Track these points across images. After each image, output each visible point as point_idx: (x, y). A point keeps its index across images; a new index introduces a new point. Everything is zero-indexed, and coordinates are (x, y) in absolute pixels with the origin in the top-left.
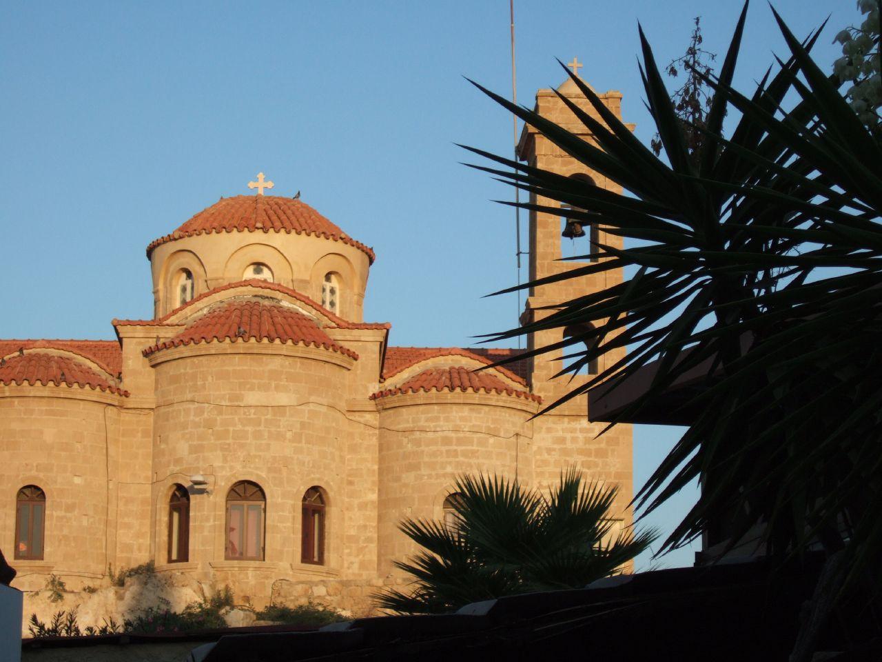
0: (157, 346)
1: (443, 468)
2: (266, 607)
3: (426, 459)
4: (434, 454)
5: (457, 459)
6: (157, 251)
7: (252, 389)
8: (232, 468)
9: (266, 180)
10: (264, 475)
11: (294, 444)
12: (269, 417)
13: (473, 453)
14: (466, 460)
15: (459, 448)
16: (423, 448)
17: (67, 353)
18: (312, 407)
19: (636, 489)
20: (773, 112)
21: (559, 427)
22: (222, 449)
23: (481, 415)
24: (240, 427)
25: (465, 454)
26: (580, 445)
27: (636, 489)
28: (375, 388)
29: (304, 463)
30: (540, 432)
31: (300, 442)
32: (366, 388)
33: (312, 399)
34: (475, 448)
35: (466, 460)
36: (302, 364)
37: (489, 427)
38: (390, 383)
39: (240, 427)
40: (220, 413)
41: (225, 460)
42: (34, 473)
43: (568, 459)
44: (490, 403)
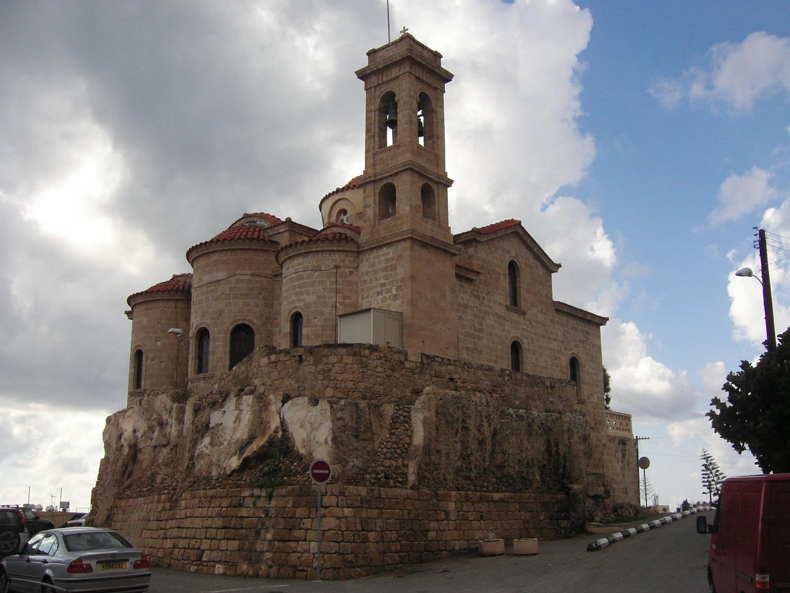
2: (65, 505)
5: (296, 291)
11: (225, 301)
12: (212, 288)
16: (203, 297)
17: (463, 274)
18: (237, 277)
19: (744, 464)
21: (372, 256)
23: (309, 259)
26: (383, 265)
27: (744, 464)
29: (231, 311)
30: (362, 262)
33: (237, 273)
34: (305, 281)
36: (231, 253)
37: (314, 266)
43: (376, 276)
44: (311, 250)
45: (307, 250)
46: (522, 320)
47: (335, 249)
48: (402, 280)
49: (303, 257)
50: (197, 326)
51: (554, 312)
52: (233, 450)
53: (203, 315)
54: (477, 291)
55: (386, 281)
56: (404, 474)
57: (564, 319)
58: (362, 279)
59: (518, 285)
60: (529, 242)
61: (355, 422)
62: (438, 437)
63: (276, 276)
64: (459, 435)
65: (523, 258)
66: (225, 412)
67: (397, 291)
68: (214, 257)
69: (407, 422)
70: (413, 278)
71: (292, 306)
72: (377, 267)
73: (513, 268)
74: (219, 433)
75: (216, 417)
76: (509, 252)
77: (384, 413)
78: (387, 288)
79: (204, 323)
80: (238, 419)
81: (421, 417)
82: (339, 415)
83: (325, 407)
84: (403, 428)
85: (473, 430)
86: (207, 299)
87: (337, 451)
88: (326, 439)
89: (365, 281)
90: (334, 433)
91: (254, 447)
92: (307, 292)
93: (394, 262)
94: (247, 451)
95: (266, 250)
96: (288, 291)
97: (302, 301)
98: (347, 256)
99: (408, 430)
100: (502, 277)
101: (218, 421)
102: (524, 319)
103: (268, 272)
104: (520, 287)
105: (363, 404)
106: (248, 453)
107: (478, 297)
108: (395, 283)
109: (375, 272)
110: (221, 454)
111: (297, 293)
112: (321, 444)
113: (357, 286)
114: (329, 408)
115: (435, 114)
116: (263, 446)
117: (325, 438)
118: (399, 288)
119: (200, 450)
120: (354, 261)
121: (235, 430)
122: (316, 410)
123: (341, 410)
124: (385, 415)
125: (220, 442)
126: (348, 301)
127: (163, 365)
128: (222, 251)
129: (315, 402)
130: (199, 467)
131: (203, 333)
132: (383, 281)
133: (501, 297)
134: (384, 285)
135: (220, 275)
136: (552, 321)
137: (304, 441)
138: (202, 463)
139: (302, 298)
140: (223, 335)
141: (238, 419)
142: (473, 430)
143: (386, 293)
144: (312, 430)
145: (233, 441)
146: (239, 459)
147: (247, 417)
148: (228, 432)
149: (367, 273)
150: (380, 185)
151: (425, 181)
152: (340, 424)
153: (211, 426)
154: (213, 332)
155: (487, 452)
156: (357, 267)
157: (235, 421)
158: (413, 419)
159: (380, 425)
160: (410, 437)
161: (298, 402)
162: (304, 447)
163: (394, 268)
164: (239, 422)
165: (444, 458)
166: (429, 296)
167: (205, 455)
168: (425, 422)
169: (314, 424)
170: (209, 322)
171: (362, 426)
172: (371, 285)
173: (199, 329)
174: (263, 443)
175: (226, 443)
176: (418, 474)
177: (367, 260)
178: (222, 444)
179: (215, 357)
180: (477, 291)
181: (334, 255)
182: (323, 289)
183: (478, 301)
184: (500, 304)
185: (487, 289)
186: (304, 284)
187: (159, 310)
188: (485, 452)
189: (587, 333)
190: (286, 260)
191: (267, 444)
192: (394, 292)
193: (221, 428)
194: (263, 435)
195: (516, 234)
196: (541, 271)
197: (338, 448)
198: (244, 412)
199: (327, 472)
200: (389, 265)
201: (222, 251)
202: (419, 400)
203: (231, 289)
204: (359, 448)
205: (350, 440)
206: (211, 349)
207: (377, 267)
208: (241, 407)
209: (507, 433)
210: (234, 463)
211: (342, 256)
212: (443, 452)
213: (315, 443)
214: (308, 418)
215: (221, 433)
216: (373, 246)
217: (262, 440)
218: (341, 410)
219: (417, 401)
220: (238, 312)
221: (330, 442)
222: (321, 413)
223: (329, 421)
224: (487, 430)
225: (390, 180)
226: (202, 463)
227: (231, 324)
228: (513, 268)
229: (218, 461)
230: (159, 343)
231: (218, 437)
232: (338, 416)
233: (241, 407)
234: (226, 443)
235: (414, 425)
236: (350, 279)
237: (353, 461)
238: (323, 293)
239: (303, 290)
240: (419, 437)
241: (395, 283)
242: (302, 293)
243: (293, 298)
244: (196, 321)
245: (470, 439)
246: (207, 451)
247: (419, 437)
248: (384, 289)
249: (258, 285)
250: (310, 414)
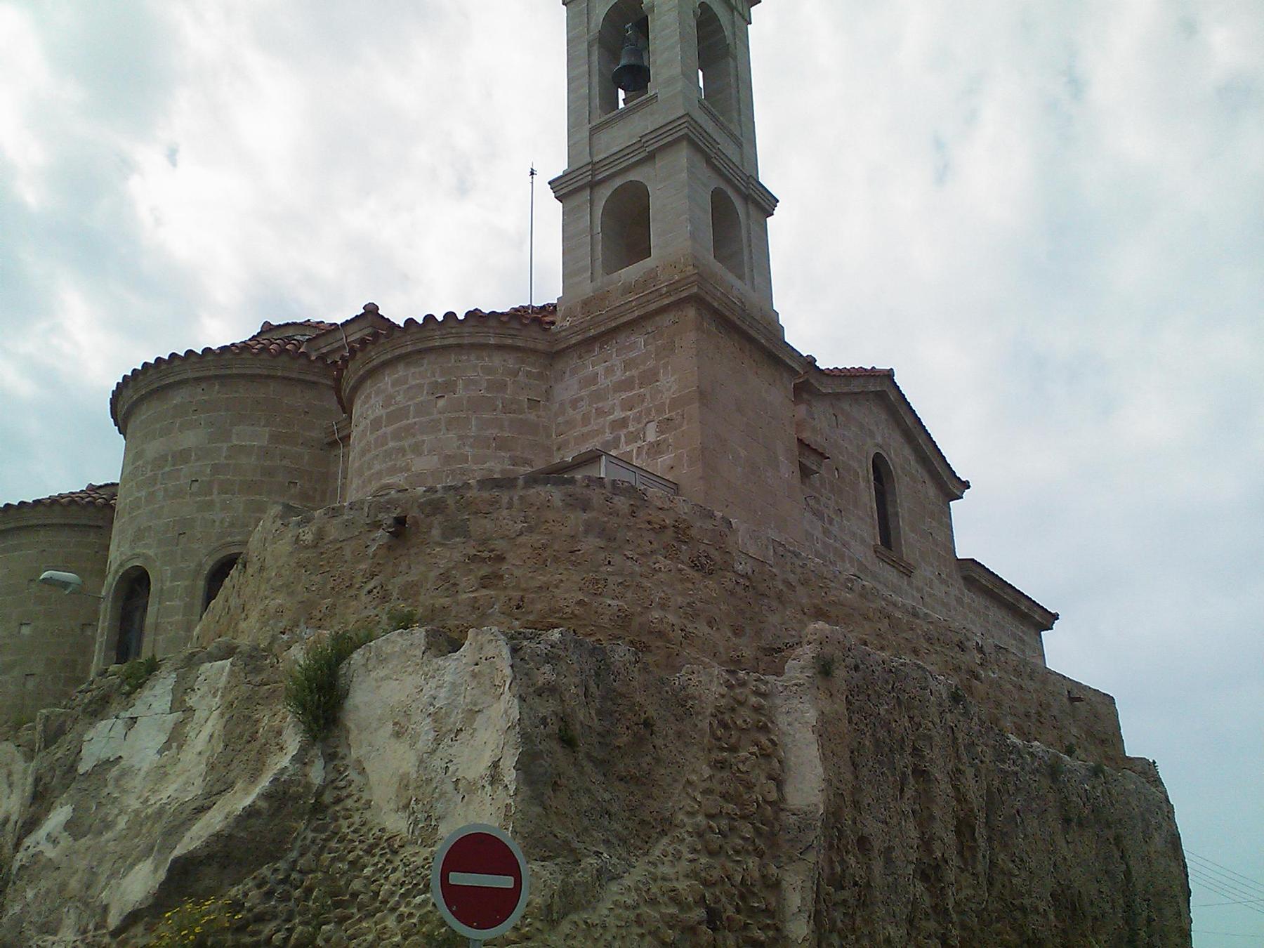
15: (390, 429)
26: (619, 375)
43: (600, 405)
44: (431, 344)
45: (420, 346)
46: (905, 586)
47: (492, 341)
48: (675, 404)
49: (408, 365)
50: (121, 565)
51: (962, 581)
52: (142, 842)
53: (139, 536)
54: (818, 501)
55: (629, 413)
56: (768, 912)
57: (979, 602)
58: (560, 419)
59: (890, 510)
60: (909, 421)
61: (599, 712)
62: (856, 790)
63: (333, 444)
64: (909, 793)
65: (900, 457)
66: (134, 720)
67: (661, 432)
68: (178, 398)
69: (764, 729)
70: (703, 396)
71: (375, 485)
72: (604, 382)
73: (880, 469)
74: (106, 791)
75: (99, 741)
76: (872, 434)
77: (690, 691)
78: (631, 429)
79: (138, 556)
80: (176, 739)
81: (811, 716)
82: (545, 674)
83: (490, 650)
84: (755, 749)
85: (943, 787)
86: (151, 497)
87: (539, 810)
88: (495, 765)
89: (570, 423)
90: (526, 737)
91: (214, 821)
92: (417, 449)
93: (651, 363)
94: (186, 839)
95: (314, 383)
96: (363, 453)
97: (401, 470)
98: (523, 362)
99: (767, 756)
100: (862, 484)
101: (108, 753)
102: (910, 584)
103: (316, 434)
104: (897, 514)
105: (621, 654)
106: (192, 840)
107: (818, 514)
108: (653, 413)
109: (598, 396)
110: (100, 862)
112: (472, 788)
113: (549, 436)
114: (506, 652)
115: (732, 63)
116: (251, 812)
117: (487, 761)
118: (665, 425)
119: (32, 851)
120: (540, 376)
121: (160, 774)
122: (453, 666)
123: (550, 659)
124: (693, 698)
125: (103, 820)
127: (31, 684)
128: (198, 380)
129: (446, 642)
130: (17, 909)
131: (136, 585)
132: (618, 414)
133: (860, 528)
134: (623, 423)
135: (190, 439)
136: (959, 600)
137: (404, 783)
138: (30, 894)
139: (401, 463)
140: (187, 583)
141: (176, 739)
142: (943, 787)
143: (627, 443)
144: (438, 741)
145: (150, 811)
146: (156, 870)
147: (207, 728)
148: (136, 783)
149: (574, 403)
150: (605, 193)
151: (723, 186)
152: (547, 707)
153: (82, 768)
155: (980, 855)
156: (548, 393)
157: (167, 746)
158: (782, 720)
159: (679, 735)
160: (780, 784)
161: (388, 649)
162: (407, 806)
163: (650, 378)
164: (180, 747)
165: (878, 866)
166: (743, 453)
167: (45, 867)
168: (824, 732)
169: (447, 715)
170: (151, 553)
171: (620, 729)
172: (585, 430)
173: (126, 573)
174: (248, 801)
175: (122, 823)
176: (817, 917)
177: (574, 372)
178: (108, 826)
179: (160, 638)
180: (818, 501)
181: (489, 356)
182: (460, 438)
183: (819, 523)
184: (863, 541)
185: (837, 502)
186: (408, 429)
188: (974, 856)
189: (1022, 641)
190: (362, 381)
191: (263, 804)
192: (651, 436)
193: (115, 771)
194: (254, 778)
195: (881, 397)
196: (931, 491)
197: (538, 798)
198: (200, 715)
199: (507, 882)
200: (635, 372)
201: (198, 380)
202: (797, 658)
203: (216, 469)
204: (615, 808)
205: (581, 773)
206: (150, 619)
207: (604, 382)
208: (192, 700)
209: (1018, 805)
210: (140, 883)
211: (511, 361)
212: (877, 845)
213: (449, 787)
214: (425, 699)
215: (110, 788)
216: (592, 333)
217: (247, 794)
218: (550, 659)
219: (790, 663)
220: (232, 525)
221: (510, 775)
222: (474, 675)
223: (507, 695)
224: (974, 791)
225: (633, 176)
226: (30, 894)
227: (209, 555)
228: (880, 469)
229: (88, 887)
230: (26, 630)
231: (99, 804)
232: (541, 681)
233: (192, 700)
234: (122, 823)
235: (788, 740)
236: (532, 417)
237: (598, 854)
238: (459, 448)
240: (807, 784)
241: (653, 413)
242: (402, 451)
243: (377, 467)
244: (119, 554)
245: (937, 812)
246: (51, 852)
247: (807, 784)
248: (623, 433)
249: (286, 462)
250: (433, 683)
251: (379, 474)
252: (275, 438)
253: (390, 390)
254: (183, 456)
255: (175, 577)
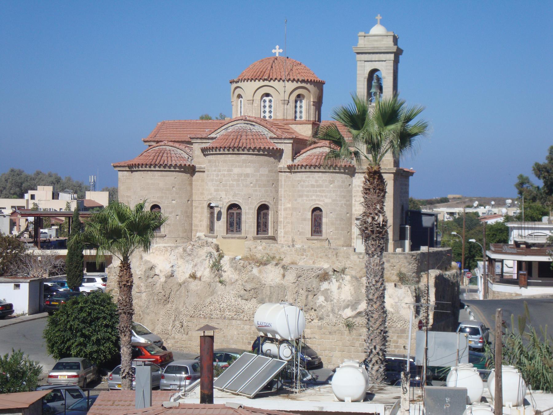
0: (22, 184)
1: (311, 197)
3: (306, 193)
4: (308, 191)
6: (238, 89)
7: (236, 167)
8: (228, 198)
9: (275, 49)
10: (241, 201)
13: (323, 191)
14: (320, 194)
15: (318, 189)
20: (421, 221)
22: (225, 191)
24: (231, 182)
25: (320, 191)
28: (290, 162)
31: (256, 187)
32: (287, 162)
35: (320, 194)
38: (296, 162)
39: (231, 182)
40: (224, 177)
41: (226, 195)
42: (156, 200)
68: (244, 157)
92: (326, 196)
111: (317, 196)
126: (348, 203)
154: (245, 209)
187: (173, 178)
203: (257, 180)
239: (323, 194)
243: (314, 198)
251: (315, 200)
252: (269, 171)
253: (317, 179)
254: (247, 175)
255: (249, 209)
